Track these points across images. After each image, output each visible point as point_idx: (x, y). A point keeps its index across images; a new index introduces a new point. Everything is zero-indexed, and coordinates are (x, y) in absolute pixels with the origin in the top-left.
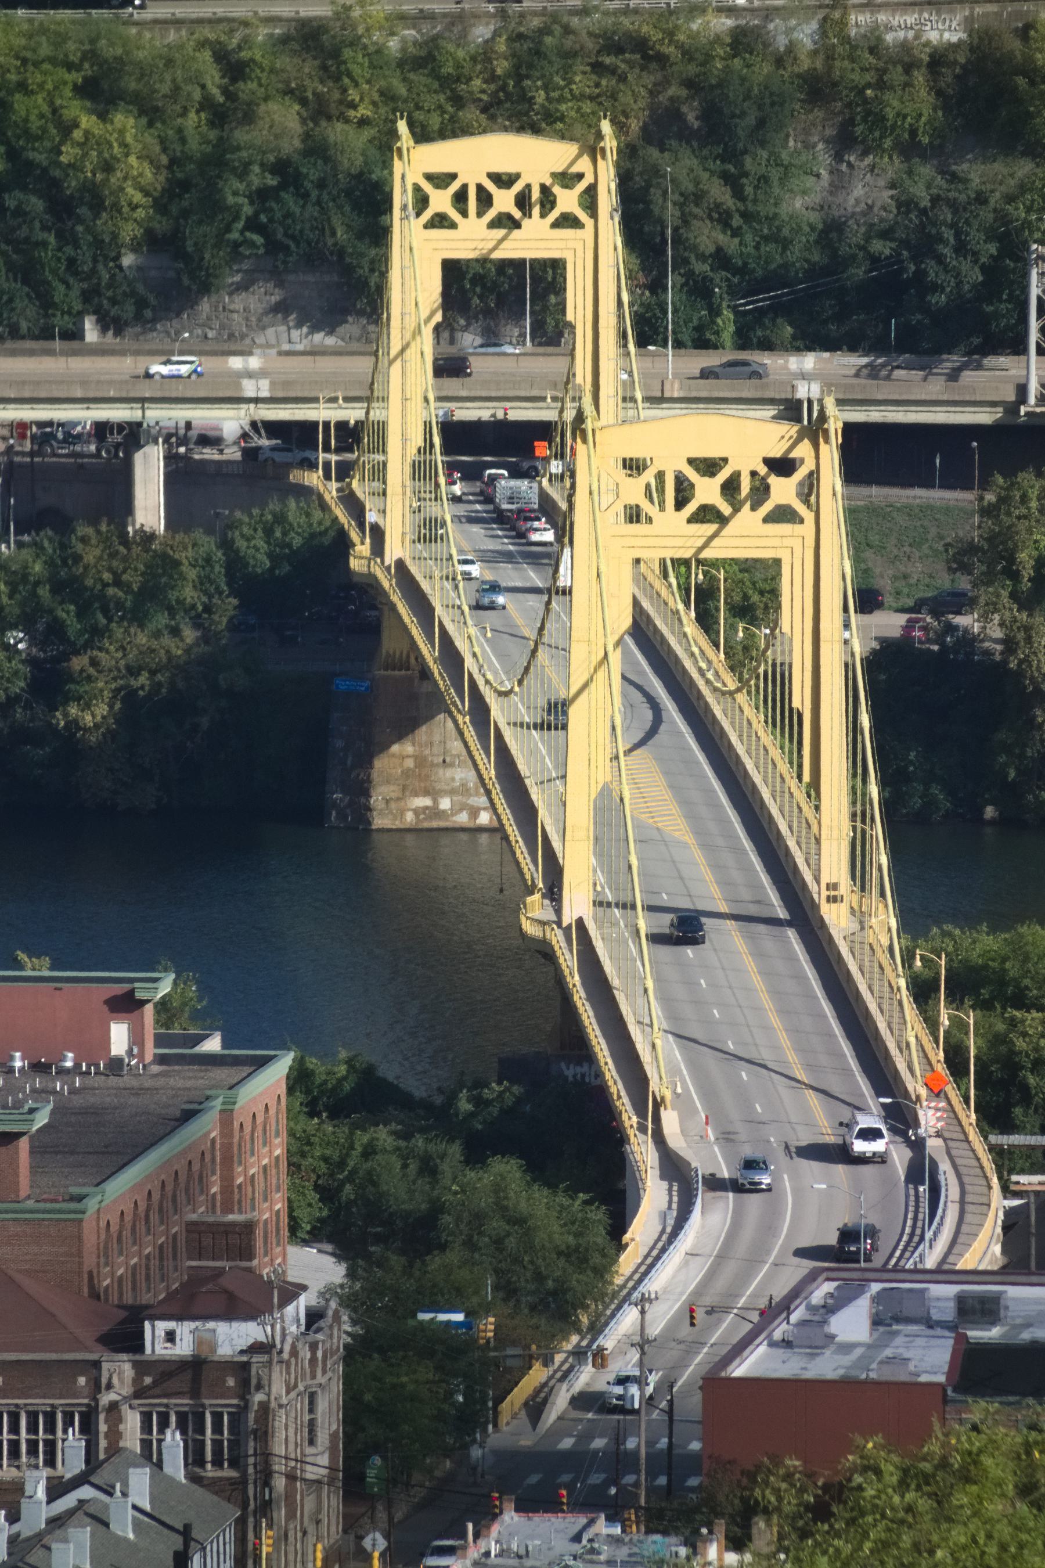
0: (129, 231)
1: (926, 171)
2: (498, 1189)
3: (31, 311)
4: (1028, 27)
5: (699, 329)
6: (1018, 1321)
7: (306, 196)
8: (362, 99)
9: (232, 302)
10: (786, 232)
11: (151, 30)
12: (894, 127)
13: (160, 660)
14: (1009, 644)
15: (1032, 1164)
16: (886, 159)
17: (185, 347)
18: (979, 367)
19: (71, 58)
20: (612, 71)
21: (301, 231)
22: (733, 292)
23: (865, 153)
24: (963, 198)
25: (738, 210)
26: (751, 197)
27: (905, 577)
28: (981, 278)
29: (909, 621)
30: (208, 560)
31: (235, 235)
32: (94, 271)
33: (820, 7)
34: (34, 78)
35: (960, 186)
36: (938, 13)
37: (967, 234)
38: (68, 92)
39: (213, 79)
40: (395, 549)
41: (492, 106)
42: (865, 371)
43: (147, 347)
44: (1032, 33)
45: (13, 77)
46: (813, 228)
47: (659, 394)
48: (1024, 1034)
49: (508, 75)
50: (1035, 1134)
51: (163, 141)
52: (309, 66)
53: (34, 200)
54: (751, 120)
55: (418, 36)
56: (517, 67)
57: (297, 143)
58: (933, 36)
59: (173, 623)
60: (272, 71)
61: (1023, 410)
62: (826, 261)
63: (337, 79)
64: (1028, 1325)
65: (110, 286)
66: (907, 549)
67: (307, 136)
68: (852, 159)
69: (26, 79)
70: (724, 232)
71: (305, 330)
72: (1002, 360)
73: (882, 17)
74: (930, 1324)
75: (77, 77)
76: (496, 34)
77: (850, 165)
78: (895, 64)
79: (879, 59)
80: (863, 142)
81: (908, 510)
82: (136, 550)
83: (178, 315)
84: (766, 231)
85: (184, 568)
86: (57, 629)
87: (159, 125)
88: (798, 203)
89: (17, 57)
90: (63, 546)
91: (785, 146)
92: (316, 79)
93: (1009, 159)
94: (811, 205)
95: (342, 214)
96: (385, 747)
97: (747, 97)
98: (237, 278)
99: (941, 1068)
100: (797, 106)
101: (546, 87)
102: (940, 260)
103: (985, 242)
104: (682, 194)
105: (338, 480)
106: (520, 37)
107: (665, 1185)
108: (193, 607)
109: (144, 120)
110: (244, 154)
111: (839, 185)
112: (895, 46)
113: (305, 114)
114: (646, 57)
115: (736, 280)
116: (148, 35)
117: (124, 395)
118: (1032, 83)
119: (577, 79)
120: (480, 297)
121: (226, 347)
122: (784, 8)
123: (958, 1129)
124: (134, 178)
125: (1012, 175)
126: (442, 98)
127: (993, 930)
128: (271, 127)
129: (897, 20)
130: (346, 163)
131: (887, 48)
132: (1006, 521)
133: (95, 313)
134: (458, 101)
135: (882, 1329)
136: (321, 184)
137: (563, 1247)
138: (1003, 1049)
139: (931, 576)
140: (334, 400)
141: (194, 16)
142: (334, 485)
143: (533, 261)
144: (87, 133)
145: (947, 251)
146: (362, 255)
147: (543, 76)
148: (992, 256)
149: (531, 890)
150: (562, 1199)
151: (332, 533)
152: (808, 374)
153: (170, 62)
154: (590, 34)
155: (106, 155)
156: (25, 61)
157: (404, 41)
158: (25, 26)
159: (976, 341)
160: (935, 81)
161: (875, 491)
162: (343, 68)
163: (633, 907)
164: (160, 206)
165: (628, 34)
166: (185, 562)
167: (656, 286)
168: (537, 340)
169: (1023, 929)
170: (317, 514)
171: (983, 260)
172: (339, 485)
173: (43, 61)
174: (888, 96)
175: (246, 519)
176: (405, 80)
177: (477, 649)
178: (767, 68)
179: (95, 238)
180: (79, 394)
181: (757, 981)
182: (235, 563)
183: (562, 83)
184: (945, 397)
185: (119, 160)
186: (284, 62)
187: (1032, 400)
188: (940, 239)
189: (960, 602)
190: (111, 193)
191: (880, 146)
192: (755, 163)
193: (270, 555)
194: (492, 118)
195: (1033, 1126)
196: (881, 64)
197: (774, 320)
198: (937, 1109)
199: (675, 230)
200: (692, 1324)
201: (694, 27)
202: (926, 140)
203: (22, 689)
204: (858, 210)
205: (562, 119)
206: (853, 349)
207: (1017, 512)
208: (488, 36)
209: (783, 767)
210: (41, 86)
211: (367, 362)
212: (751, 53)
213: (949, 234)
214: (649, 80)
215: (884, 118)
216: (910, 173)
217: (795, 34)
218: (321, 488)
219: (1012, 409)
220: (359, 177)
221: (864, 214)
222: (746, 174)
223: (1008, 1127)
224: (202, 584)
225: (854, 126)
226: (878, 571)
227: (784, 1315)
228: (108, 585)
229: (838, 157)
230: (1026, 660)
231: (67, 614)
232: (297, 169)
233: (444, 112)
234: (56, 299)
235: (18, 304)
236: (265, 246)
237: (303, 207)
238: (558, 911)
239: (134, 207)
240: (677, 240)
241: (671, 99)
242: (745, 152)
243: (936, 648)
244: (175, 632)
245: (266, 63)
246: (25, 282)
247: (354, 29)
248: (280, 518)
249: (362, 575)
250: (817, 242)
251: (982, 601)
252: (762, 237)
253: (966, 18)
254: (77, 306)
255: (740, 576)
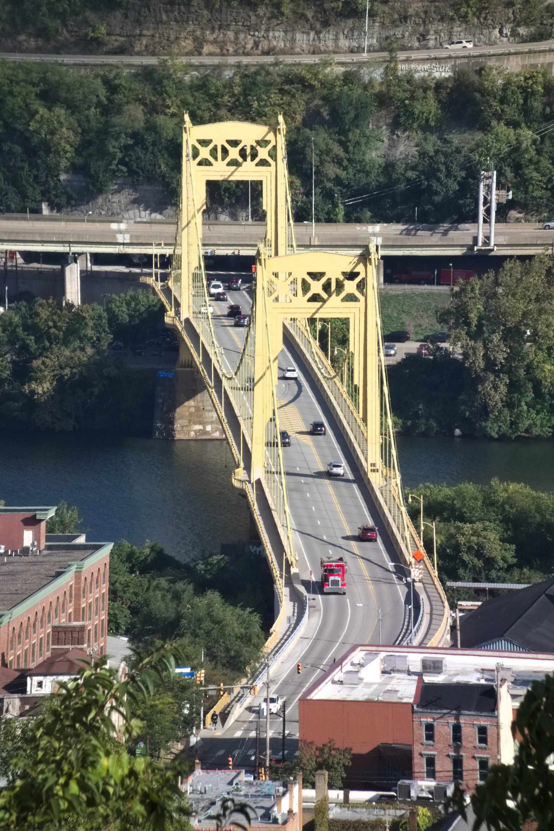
0: (64, 163)
1: (433, 138)
2: (209, 605)
3: (17, 199)
4: (482, 69)
5: (328, 213)
6: (452, 673)
7: (147, 149)
8: (172, 104)
9: (112, 198)
10: (367, 168)
11: (73, 68)
12: (418, 118)
13: (76, 362)
14: (466, 355)
15: (469, 596)
16: (415, 134)
17: (91, 218)
18: (457, 229)
19: (34, 80)
20: (288, 92)
21: (145, 166)
22: (343, 196)
23: (405, 131)
24: (450, 150)
25: (346, 158)
26: (352, 151)
27: (420, 326)
28: (457, 188)
29: (421, 346)
30: (100, 317)
31: (113, 167)
32: (47, 181)
33: (384, 61)
34: (16, 89)
35: (449, 145)
36: (440, 63)
37: (452, 168)
38: (33, 96)
39: (103, 93)
40: (185, 314)
41: (233, 108)
42: (404, 232)
43: (72, 218)
44: (483, 72)
45: (6, 88)
46: (380, 166)
47: (308, 244)
48: (463, 535)
49: (240, 94)
50: (469, 582)
51: (79, 121)
52: (148, 88)
53: (17, 147)
54: (352, 114)
55: (199, 75)
56: (245, 90)
57: (142, 124)
58: (437, 75)
59: (82, 345)
60: (130, 90)
61: (476, 248)
62: (386, 181)
63: (161, 94)
64: (457, 675)
65: (54, 189)
66: (421, 313)
67: (147, 121)
68: (399, 133)
69: (12, 89)
70: (340, 168)
71: (148, 212)
72: (467, 226)
73: (413, 66)
74: (409, 673)
75: (37, 90)
76: (235, 74)
77: (398, 136)
78: (419, 88)
79: (411, 86)
80: (403, 125)
81: (421, 295)
82: (65, 312)
83: (88, 203)
84: (359, 167)
85: (87, 321)
86: (25, 347)
87: (77, 114)
88: (374, 154)
89: (8, 79)
90: (31, 309)
91: (368, 128)
92: (151, 94)
93: (472, 132)
94: (380, 155)
95: (164, 158)
96: (181, 403)
97: (350, 104)
98: (116, 187)
99: (422, 551)
100: (373, 109)
101: (258, 100)
102: (438, 180)
103: (460, 171)
104: (320, 151)
105: (161, 281)
106: (246, 76)
107: (292, 604)
108: (92, 338)
109: (69, 111)
110: (117, 129)
111: (393, 145)
112: (419, 80)
113: (146, 111)
114: (304, 86)
115: (344, 191)
116: (71, 71)
117: (60, 240)
118: (483, 96)
119: (272, 96)
120: (228, 198)
121: (110, 219)
122: (367, 62)
123: (430, 578)
124: (66, 138)
125: (473, 139)
126: (210, 104)
127: (449, 485)
128: (130, 116)
129: (420, 67)
130: (165, 135)
131: (416, 81)
132: (465, 300)
133: (47, 201)
134: (217, 106)
135: (386, 675)
136: (154, 144)
137: (239, 635)
138: (453, 542)
139: (432, 325)
140: (160, 244)
141: (93, 63)
142: (160, 284)
143: (252, 181)
144: (42, 116)
145: (442, 176)
146: (173, 178)
147: (257, 95)
148: (463, 177)
149: (238, 466)
150: (238, 610)
151: (158, 306)
152: (377, 234)
153: (82, 84)
154: (279, 75)
155: (51, 127)
156: (11, 81)
157: (192, 76)
158: (12, 65)
159: (455, 217)
160: (437, 96)
161: (406, 287)
162: (163, 89)
163: (280, 473)
164: (78, 151)
165: (295, 75)
166: (87, 317)
167: (308, 194)
168: (254, 218)
169: (462, 486)
170: (151, 297)
171: (459, 179)
172: (162, 284)
173: (21, 81)
174: (416, 103)
175: (117, 298)
176: (192, 95)
177: (219, 359)
178: (360, 91)
179: (47, 166)
180: (38, 239)
181: (338, 508)
182: (113, 318)
183: (266, 98)
184: (440, 243)
185: (57, 130)
186: (136, 86)
187: (480, 244)
188: (439, 170)
189: (444, 338)
190: (54, 145)
191: (411, 127)
192: (354, 135)
193: (129, 315)
194: (233, 114)
195: (469, 578)
196: (412, 88)
197: (361, 210)
198: (420, 569)
199: (317, 167)
200: (299, 673)
201: (326, 71)
202: (433, 124)
203: (8, 375)
204: (401, 157)
205: (265, 115)
206: (398, 222)
207: (470, 296)
208: (231, 75)
209: (352, 408)
210: (20, 93)
211: (173, 227)
212: (352, 84)
213: (443, 168)
214: (306, 97)
215: (413, 114)
216: (425, 139)
217: (373, 75)
218: (154, 285)
219: (470, 248)
220: (171, 141)
221: (404, 159)
222: (350, 141)
223: (457, 578)
224: (96, 327)
225: (400, 117)
226: (407, 323)
227: (340, 668)
228: (51, 327)
229: (393, 133)
230: (474, 362)
231: (31, 340)
232: (142, 136)
233: (211, 111)
234: (29, 194)
235: (9, 195)
236: (127, 172)
237: (145, 154)
238: (249, 476)
239: (66, 152)
240: (318, 172)
241: (316, 106)
242: (349, 130)
243: (432, 357)
244: (83, 349)
245: (127, 85)
246: (14, 185)
247: (169, 70)
248: (134, 298)
249: (170, 325)
250: (382, 172)
251: (453, 336)
252: (357, 170)
253: (452, 66)
254: (39, 198)
255: (342, 326)
